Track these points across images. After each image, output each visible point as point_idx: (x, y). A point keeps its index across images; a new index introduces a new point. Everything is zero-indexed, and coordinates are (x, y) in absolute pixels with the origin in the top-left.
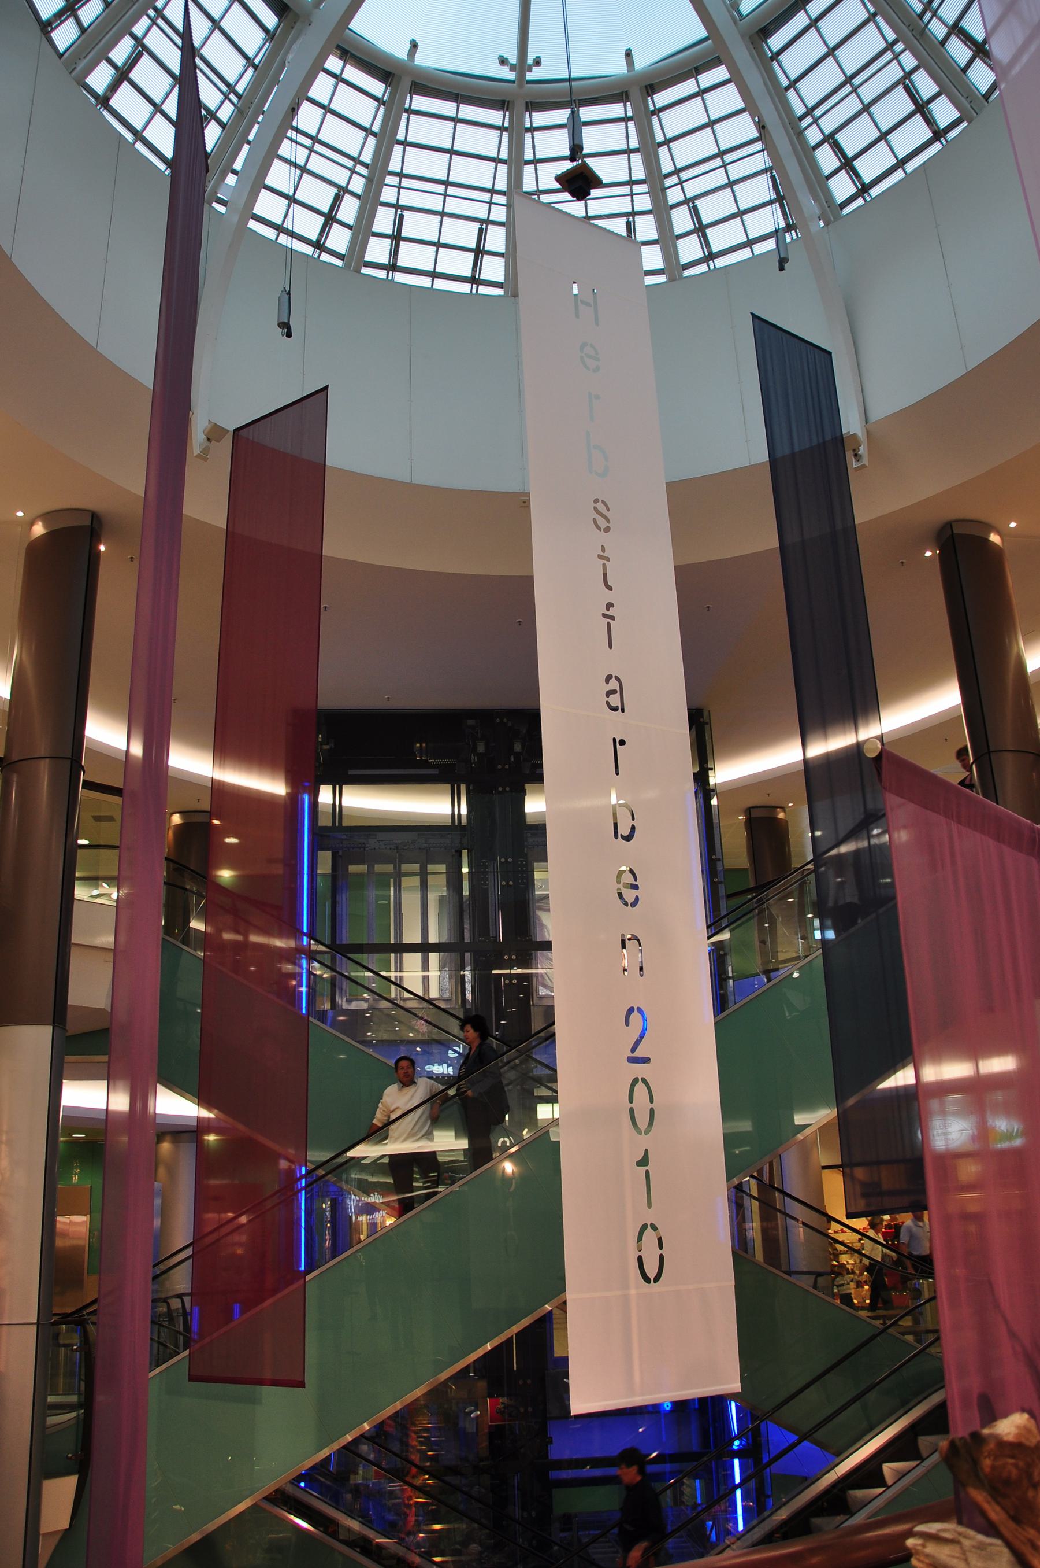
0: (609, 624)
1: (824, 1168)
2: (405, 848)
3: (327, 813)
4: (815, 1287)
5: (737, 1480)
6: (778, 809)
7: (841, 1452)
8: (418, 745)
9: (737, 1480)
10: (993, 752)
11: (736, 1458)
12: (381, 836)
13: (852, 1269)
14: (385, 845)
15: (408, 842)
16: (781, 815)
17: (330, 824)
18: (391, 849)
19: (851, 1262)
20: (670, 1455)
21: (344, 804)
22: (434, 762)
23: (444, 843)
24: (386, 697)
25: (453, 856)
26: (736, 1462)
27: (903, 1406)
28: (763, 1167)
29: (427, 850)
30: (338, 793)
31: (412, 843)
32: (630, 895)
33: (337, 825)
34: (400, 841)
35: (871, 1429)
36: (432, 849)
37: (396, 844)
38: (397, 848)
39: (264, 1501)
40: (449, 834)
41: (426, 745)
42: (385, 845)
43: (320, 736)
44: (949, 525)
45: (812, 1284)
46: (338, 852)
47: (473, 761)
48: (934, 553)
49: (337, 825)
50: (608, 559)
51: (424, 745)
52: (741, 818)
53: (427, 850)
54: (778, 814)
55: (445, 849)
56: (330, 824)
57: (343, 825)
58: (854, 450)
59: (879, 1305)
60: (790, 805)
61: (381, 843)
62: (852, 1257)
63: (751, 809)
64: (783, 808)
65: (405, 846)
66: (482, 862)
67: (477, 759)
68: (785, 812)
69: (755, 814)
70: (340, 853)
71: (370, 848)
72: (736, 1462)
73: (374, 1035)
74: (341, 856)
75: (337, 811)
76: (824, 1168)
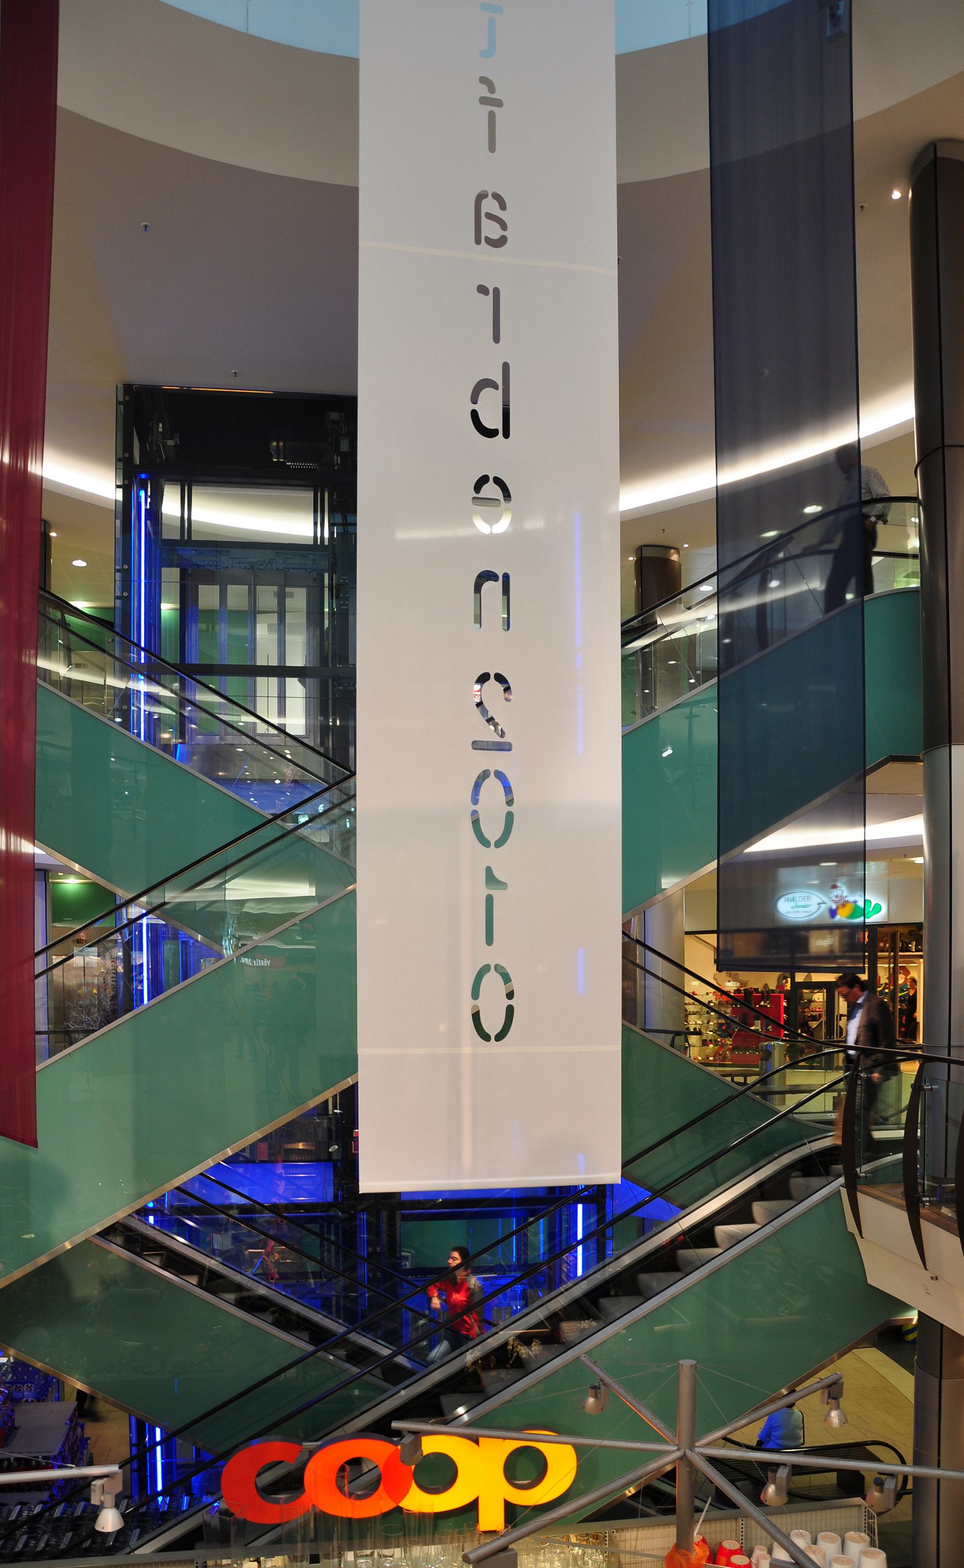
0: (492, 116)
1: (687, 933)
2: (261, 567)
3: (174, 527)
4: (672, 1045)
5: (580, 1236)
6: (672, 551)
7: (685, 1206)
8: (275, 444)
9: (580, 1236)
10: (947, 446)
11: (580, 1203)
12: (234, 552)
13: (700, 1029)
14: (239, 563)
15: (265, 561)
16: (675, 557)
17: (179, 538)
18: (245, 568)
19: (699, 1022)
20: (517, 1199)
21: (193, 518)
22: (293, 466)
23: (305, 564)
24: (233, 371)
25: (315, 579)
26: (580, 1207)
27: (753, 1164)
28: (631, 919)
29: (285, 571)
30: (186, 501)
31: (269, 562)
32: (491, 230)
33: (186, 538)
34: (255, 560)
35: (718, 1185)
36: (291, 570)
37: (251, 563)
38: (252, 567)
39: (97, 1236)
40: (310, 554)
41: (284, 444)
42: (239, 563)
43: (161, 425)
44: (933, 146)
45: (669, 1042)
46: (187, 570)
47: (335, 463)
48: (905, 196)
49: (186, 538)
50: (499, 103)
51: (281, 444)
52: (631, 559)
53: (285, 571)
54: (672, 555)
55: (306, 571)
56: (179, 538)
57: (192, 539)
58: (832, 8)
59: (845, 1093)
60: (686, 546)
61: (235, 560)
62: (700, 1018)
63: (643, 548)
64: (677, 550)
65: (261, 565)
66: (342, 579)
67: (341, 461)
68: (679, 554)
69: (647, 553)
70: (190, 571)
71: (222, 566)
72: (580, 1207)
73: (256, 802)
74: (190, 575)
75: (186, 524)
76: (687, 933)
